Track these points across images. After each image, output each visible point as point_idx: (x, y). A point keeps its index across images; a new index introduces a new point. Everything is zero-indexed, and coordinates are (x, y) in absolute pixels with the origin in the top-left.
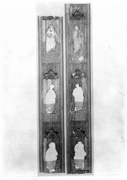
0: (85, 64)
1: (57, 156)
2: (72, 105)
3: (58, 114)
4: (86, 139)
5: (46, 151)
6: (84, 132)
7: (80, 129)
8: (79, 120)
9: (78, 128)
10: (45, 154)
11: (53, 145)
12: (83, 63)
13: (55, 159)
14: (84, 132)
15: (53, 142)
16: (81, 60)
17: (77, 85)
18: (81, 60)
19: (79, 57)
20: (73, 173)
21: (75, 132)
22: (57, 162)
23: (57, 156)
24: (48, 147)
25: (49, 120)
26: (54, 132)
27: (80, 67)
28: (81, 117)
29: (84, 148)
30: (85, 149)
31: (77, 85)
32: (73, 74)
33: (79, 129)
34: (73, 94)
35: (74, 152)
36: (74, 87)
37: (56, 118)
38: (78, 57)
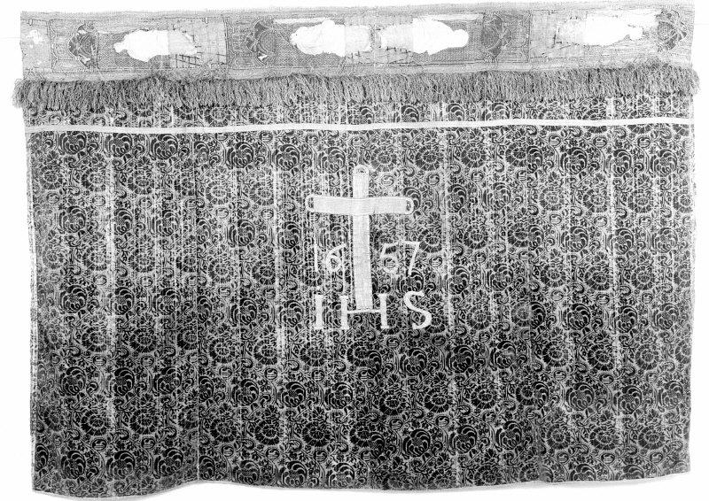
0: (53, 25)
1: (426, 52)
2: (180, 64)
3: (551, 55)
4: (280, 22)
5: (447, 23)
6: (260, 27)
7: (252, 38)
8: (223, 43)
9: (249, 45)
10: (436, 17)
11: (460, 39)
12: (51, 34)
13: (418, 49)
14: (260, 27)
15: (471, 40)
16: (41, 39)
17: (119, 47)
18: (41, 39)
19: (32, 43)
20: (407, 488)
21: (260, 55)
22: (409, 54)
23: (426, 52)
24: (454, 26)
25: (535, 26)
26: (500, 45)
27: (61, 40)
28: (213, 37)
29: (307, 25)
30: (313, 25)
31: (119, 47)
32: (86, 60)
33: (250, 42)
34: (146, 60)
35: (325, 55)
36: (124, 58)
37: (540, 51)
38: (31, 46)
